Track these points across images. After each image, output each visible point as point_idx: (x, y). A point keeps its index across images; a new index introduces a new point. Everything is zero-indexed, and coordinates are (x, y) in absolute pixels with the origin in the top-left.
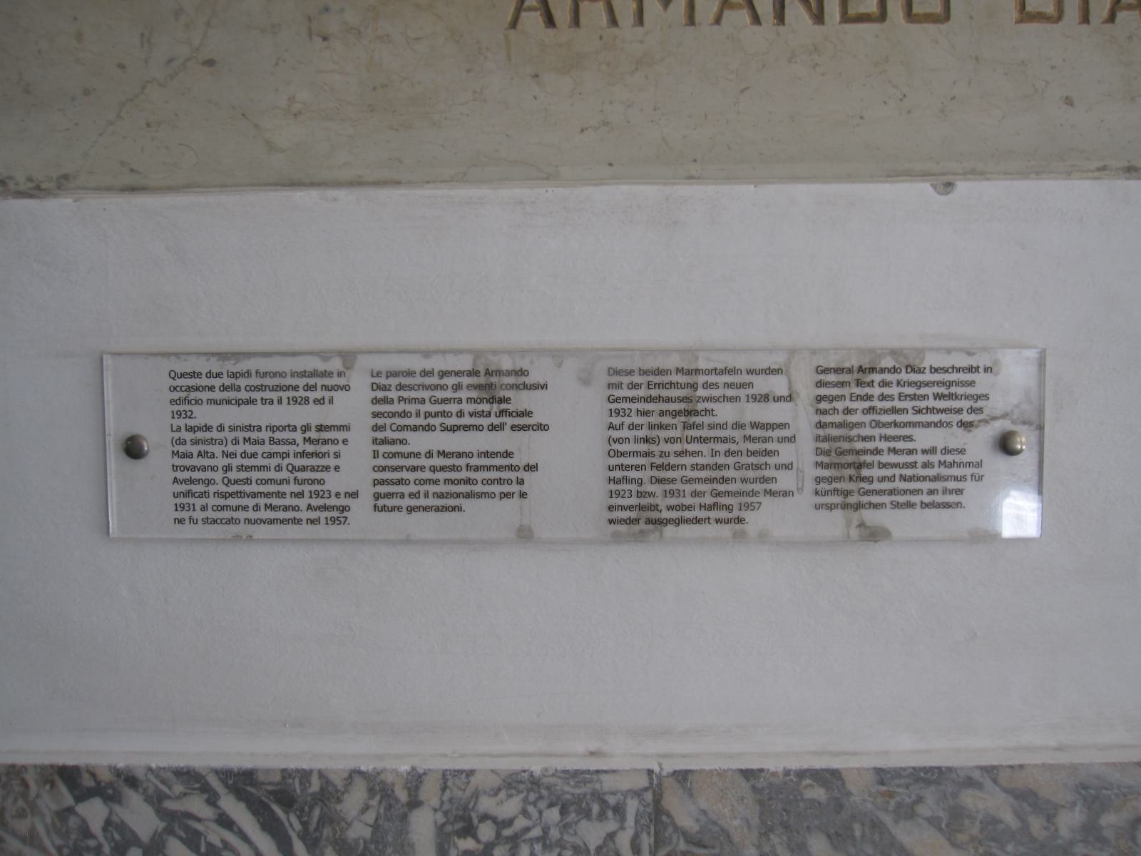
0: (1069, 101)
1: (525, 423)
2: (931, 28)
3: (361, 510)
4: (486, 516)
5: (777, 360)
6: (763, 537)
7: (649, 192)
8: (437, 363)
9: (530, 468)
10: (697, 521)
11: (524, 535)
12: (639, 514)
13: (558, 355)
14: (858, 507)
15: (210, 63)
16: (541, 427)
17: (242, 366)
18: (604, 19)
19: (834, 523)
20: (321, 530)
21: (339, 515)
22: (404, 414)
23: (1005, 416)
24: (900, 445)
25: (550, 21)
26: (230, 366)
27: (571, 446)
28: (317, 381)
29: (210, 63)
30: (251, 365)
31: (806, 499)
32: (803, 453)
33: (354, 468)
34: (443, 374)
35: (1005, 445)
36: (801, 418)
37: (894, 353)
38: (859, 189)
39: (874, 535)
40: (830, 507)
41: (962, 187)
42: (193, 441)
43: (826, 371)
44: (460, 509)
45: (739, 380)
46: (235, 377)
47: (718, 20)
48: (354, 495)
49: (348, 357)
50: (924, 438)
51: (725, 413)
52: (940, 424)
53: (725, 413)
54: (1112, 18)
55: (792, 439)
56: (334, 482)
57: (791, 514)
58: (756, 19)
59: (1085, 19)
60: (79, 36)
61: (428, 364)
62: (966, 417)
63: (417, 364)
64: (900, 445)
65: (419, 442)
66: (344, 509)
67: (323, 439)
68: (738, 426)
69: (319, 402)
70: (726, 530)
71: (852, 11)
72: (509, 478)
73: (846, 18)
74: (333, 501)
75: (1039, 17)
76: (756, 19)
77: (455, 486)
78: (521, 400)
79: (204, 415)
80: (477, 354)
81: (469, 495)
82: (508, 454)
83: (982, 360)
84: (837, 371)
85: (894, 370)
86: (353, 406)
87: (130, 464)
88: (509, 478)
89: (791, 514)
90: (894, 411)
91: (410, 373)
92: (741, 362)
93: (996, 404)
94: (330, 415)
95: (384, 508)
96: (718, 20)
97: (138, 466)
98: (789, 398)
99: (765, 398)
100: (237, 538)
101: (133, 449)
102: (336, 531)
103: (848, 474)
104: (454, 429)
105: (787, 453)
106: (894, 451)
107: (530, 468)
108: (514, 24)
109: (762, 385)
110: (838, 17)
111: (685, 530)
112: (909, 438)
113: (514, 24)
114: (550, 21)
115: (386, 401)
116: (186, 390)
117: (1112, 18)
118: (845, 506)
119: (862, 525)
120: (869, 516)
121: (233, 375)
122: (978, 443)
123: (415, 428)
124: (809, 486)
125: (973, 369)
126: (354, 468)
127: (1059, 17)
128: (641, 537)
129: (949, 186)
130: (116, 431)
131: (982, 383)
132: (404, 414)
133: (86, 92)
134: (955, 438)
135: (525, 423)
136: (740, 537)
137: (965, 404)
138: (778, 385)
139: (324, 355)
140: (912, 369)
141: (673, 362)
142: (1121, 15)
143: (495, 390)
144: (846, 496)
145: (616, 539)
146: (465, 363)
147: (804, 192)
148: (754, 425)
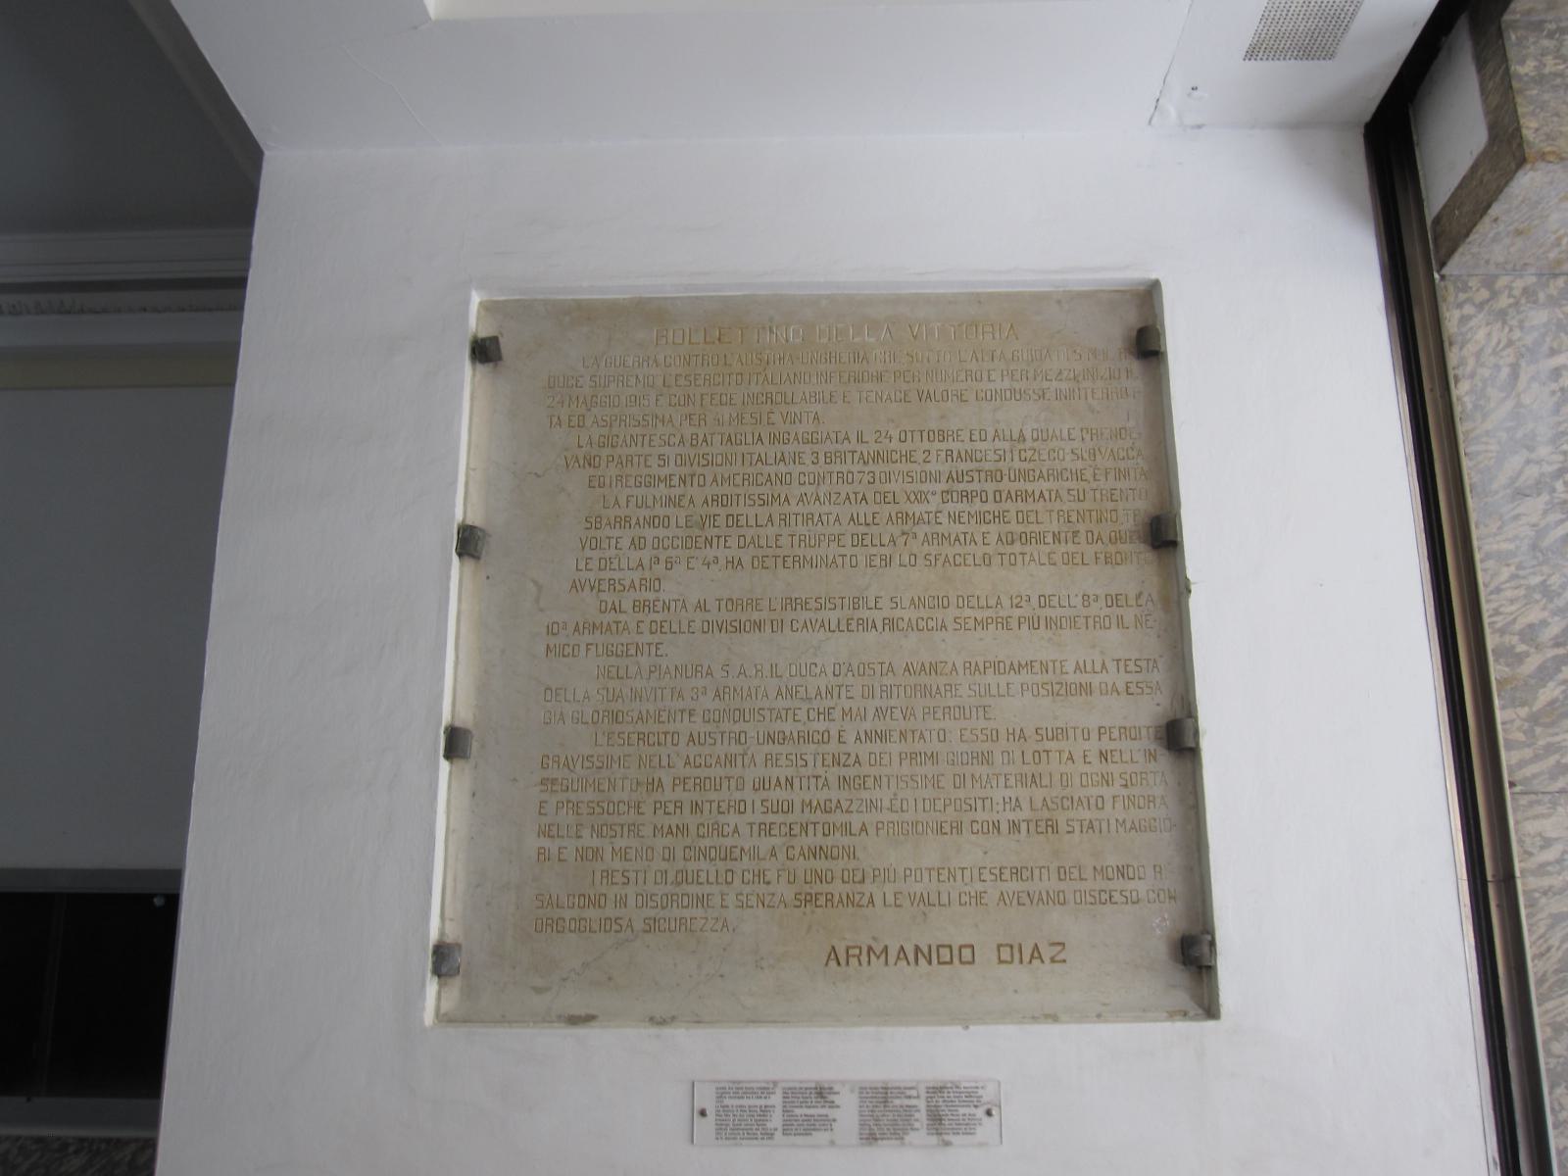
0: (1016, 991)
1: (832, 1105)
2: (968, 966)
3: (778, 1134)
4: (821, 1137)
5: (914, 1084)
6: (911, 1144)
7: (871, 1029)
8: (806, 1085)
9: (834, 1120)
10: (888, 1139)
11: (832, 1143)
12: (870, 1138)
13: (843, 1083)
14: (941, 1134)
15: (722, 976)
16: (838, 1107)
17: (740, 1085)
18: (857, 963)
19: (934, 1140)
20: (765, 1142)
21: (771, 1136)
22: (793, 1102)
23: (989, 1103)
24: (954, 1113)
25: (839, 964)
26: (736, 1085)
27: (847, 1112)
28: (766, 1090)
29: (722, 976)
30: (744, 1085)
31: (924, 1131)
32: (922, 1116)
33: (776, 1120)
34: (806, 1089)
35: (989, 1113)
36: (922, 1104)
37: (952, 1082)
38: (939, 1029)
39: (947, 1144)
40: (932, 1134)
41: (972, 1028)
42: (723, 1110)
43: (929, 1088)
44: (811, 1134)
45: (902, 1091)
46: (739, 1089)
47: (896, 964)
48: (776, 1129)
49: (775, 1083)
50: (962, 1111)
51: (897, 1102)
52: (967, 1106)
53: (897, 1102)
54: (1030, 962)
55: (919, 1111)
56: (769, 1125)
57: (920, 1136)
58: (908, 963)
59: (1021, 962)
60: (675, 965)
61: (802, 1085)
62: (976, 1103)
63: (798, 1085)
64: (954, 1113)
65: (798, 1111)
66: (772, 1134)
67: (766, 1110)
68: (901, 1106)
69: (765, 1098)
70: (898, 1142)
71: (941, 960)
72: (827, 1123)
73: (939, 963)
74: (769, 1131)
75: (1006, 962)
76: (908, 963)
77: (810, 1126)
78: (832, 1097)
79: (727, 1102)
80: (817, 1082)
81: (814, 1130)
82: (827, 1116)
83: (980, 1085)
84: (933, 1088)
85: (951, 1088)
86: (776, 1099)
87: (700, 1117)
88: (827, 1123)
89: (920, 1136)
90: (952, 1101)
91: (795, 1088)
92: (902, 1085)
93: (985, 1099)
94: (769, 1102)
95: (786, 1134)
96: (896, 964)
97: (704, 1120)
98: (918, 1097)
99: (910, 1097)
100: (736, 1145)
101: (703, 1113)
102: (769, 1142)
103: (936, 1120)
104: (809, 1107)
105: (917, 1115)
106: (952, 1115)
107: (834, 1120)
108: (827, 964)
109: (909, 1093)
110: (936, 961)
111: (885, 1142)
112: (957, 1111)
113: (827, 964)
114: (839, 964)
115: (788, 1098)
116: (721, 1094)
117: (1030, 962)
118: (937, 1134)
119: (943, 1140)
120: (946, 1137)
121: (738, 1088)
122: (980, 1112)
123: (797, 1107)
124: (925, 1126)
125: (977, 1088)
126: (776, 1120)
127: (1012, 962)
128: (870, 1144)
129: (967, 1027)
130: (697, 1106)
131: (981, 1092)
132: (793, 1102)
133: (678, 985)
134: (973, 1110)
135: (832, 1105)
136: (903, 1144)
137: (975, 1099)
138: (914, 1093)
139: (768, 1082)
140: (957, 1087)
141: (879, 1085)
142: (1034, 961)
143: (822, 1093)
144: (1559, 245)
145: (862, 1144)
146: (813, 1085)
147: (921, 1030)
148: (907, 1106)
